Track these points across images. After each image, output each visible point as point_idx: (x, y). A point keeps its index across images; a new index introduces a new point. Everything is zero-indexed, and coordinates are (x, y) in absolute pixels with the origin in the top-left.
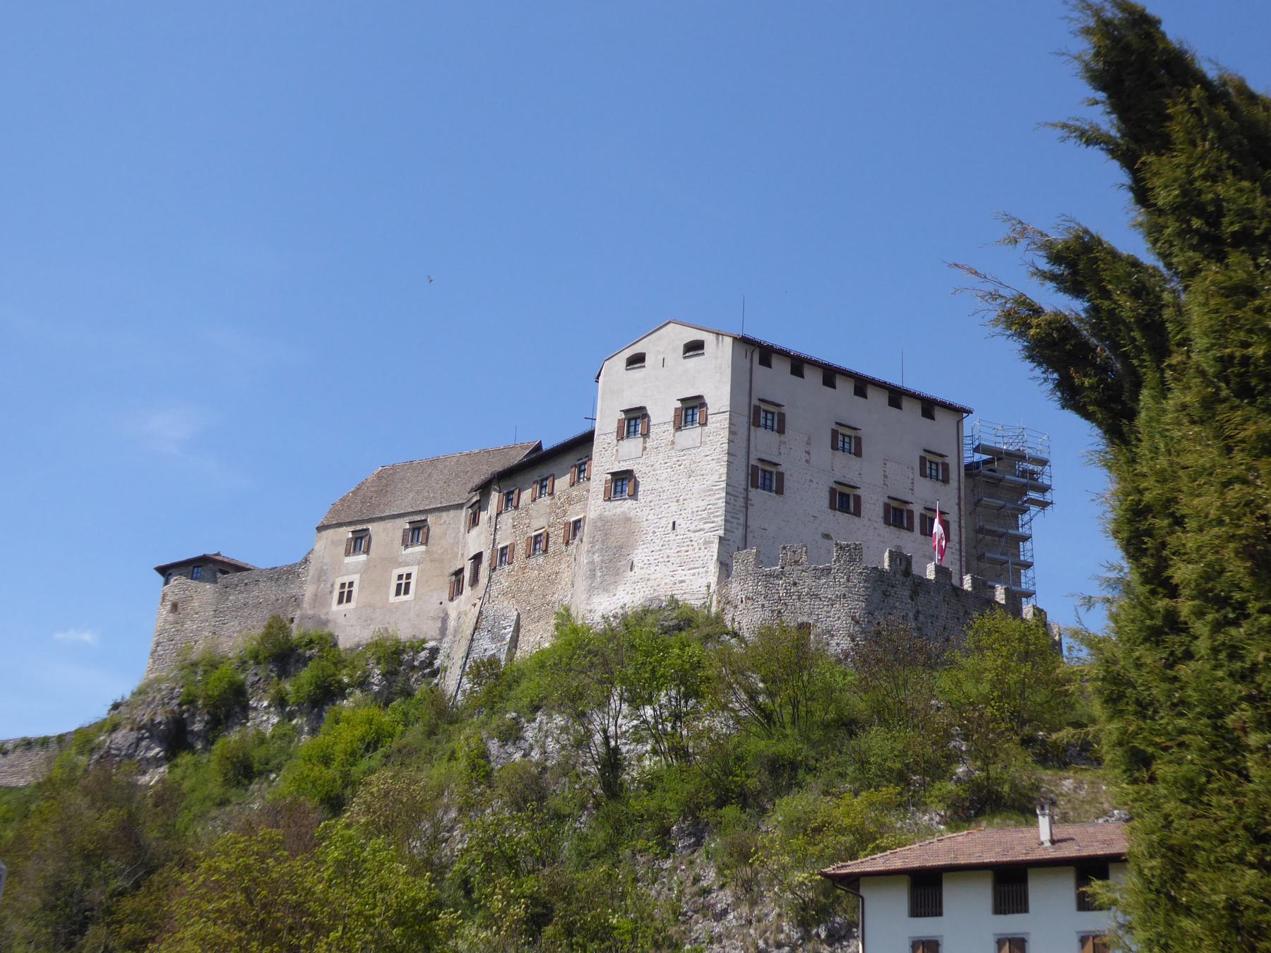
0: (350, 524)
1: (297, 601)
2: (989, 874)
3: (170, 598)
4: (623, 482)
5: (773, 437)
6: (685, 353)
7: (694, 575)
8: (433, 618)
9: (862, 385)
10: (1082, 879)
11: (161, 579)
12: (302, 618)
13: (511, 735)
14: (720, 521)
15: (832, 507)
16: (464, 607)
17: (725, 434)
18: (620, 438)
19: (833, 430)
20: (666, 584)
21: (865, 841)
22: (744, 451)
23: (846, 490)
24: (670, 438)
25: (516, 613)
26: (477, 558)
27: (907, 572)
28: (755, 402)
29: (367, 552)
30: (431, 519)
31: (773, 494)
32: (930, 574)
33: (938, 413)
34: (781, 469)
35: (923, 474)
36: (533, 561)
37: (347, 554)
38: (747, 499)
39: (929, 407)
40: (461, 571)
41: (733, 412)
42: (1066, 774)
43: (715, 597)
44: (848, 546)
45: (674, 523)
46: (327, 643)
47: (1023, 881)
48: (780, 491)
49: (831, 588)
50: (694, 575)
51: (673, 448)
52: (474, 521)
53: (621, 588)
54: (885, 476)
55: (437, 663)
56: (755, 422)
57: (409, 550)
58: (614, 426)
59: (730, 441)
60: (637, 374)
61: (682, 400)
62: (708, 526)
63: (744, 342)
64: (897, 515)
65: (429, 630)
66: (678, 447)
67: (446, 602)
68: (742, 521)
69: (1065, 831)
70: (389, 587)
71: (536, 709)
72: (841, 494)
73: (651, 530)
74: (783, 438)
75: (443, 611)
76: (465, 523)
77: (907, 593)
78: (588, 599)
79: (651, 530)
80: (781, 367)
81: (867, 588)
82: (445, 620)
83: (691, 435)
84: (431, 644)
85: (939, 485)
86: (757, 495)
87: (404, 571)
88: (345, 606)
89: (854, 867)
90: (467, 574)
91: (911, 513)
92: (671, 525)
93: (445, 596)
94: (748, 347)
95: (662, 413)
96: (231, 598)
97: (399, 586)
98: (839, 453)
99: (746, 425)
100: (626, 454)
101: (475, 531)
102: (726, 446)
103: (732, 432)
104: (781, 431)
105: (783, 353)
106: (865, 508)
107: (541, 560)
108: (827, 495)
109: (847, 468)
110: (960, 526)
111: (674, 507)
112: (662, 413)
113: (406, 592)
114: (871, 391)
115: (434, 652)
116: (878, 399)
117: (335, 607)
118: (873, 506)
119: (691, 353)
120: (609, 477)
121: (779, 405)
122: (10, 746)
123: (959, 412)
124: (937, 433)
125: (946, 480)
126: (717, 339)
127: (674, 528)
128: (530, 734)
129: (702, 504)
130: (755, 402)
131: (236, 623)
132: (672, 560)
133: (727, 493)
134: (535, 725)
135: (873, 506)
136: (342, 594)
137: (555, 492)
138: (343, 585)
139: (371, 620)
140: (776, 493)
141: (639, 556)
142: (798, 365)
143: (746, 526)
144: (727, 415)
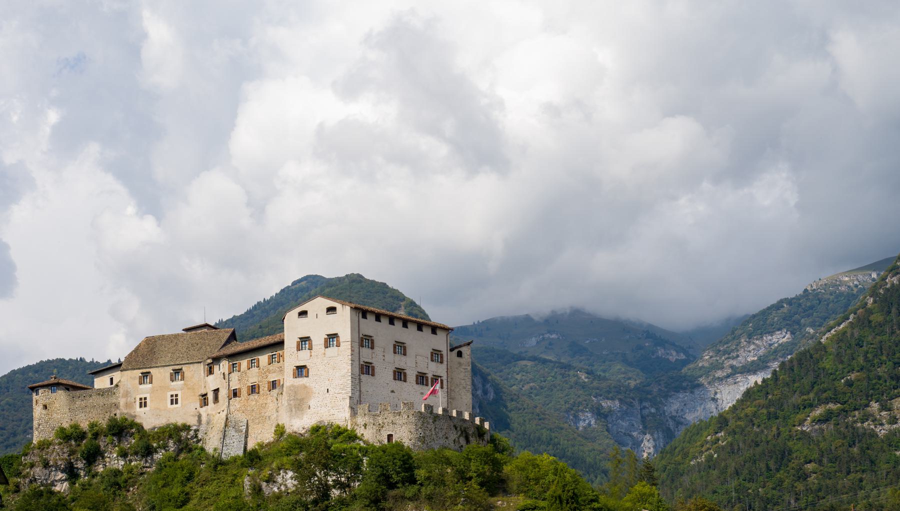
0: (139, 369)
1: (116, 406)
4: (301, 371)
5: (370, 351)
6: (327, 312)
7: (339, 412)
8: (193, 416)
13: (270, 480)
14: (349, 390)
15: (395, 379)
16: (215, 413)
17: (349, 352)
18: (298, 350)
19: (394, 345)
20: (326, 415)
22: (357, 359)
23: (400, 371)
24: (323, 352)
25: (246, 420)
26: (216, 391)
27: (431, 413)
28: (361, 336)
29: (151, 382)
31: (370, 376)
32: (440, 412)
35: (432, 360)
36: (252, 397)
37: (140, 384)
38: (360, 379)
40: (206, 395)
42: (499, 499)
44: (408, 403)
45: (328, 390)
46: (140, 428)
48: (373, 375)
49: (402, 420)
50: (339, 412)
51: (325, 356)
52: (210, 372)
53: (305, 416)
54: (416, 363)
55: (200, 436)
56: (362, 345)
57: (174, 383)
59: (352, 355)
60: (303, 320)
61: (328, 335)
62: (343, 392)
64: (422, 379)
65: (192, 421)
68: (358, 389)
70: (167, 400)
71: (279, 469)
73: (317, 392)
74: (373, 351)
75: (198, 413)
76: (204, 371)
77: (431, 421)
78: (290, 420)
79: (317, 392)
81: (416, 420)
82: (200, 416)
83: (332, 350)
84: (195, 428)
85: (439, 364)
86: (364, 377)
87: (174, 393)
88: (143, 409)
90: (211, 397)
91: (427, 377)
92: (326, 390)
95: (318, 340)
96: (77, 403)
97: (172, 400)
98: (397, 355)
99: (358, 347)
100: (303, 357)
101: (211, 377)
102: (350, 357)
103: (352, 351)
104: (372, 348)
105: (372, 312)
106: (408, 377)
108: (392, 374)
109: (401, 362)
110: (447, 381)
111: (327, 382)
112: (318, 340)
115: (197, 431)
118: (411, 376)
119: (330, 313)
120: (295, 368)
121: (371, 337)
125: (442, 362)
126: (343, 307)
127: (328, 392)
128: (279, 479)
130: (361, 336)
131: (83, 415)
132: (328, 405)
133: (352, 378)
134: (281, 476)
135: (411, 376)
136: (141, 403)
137: (260, 366)
138: (141, 399)
139: (160, 415)
140: (372, 375)
141: (312, 403)
143: (360, 391)
144: (350, 343)
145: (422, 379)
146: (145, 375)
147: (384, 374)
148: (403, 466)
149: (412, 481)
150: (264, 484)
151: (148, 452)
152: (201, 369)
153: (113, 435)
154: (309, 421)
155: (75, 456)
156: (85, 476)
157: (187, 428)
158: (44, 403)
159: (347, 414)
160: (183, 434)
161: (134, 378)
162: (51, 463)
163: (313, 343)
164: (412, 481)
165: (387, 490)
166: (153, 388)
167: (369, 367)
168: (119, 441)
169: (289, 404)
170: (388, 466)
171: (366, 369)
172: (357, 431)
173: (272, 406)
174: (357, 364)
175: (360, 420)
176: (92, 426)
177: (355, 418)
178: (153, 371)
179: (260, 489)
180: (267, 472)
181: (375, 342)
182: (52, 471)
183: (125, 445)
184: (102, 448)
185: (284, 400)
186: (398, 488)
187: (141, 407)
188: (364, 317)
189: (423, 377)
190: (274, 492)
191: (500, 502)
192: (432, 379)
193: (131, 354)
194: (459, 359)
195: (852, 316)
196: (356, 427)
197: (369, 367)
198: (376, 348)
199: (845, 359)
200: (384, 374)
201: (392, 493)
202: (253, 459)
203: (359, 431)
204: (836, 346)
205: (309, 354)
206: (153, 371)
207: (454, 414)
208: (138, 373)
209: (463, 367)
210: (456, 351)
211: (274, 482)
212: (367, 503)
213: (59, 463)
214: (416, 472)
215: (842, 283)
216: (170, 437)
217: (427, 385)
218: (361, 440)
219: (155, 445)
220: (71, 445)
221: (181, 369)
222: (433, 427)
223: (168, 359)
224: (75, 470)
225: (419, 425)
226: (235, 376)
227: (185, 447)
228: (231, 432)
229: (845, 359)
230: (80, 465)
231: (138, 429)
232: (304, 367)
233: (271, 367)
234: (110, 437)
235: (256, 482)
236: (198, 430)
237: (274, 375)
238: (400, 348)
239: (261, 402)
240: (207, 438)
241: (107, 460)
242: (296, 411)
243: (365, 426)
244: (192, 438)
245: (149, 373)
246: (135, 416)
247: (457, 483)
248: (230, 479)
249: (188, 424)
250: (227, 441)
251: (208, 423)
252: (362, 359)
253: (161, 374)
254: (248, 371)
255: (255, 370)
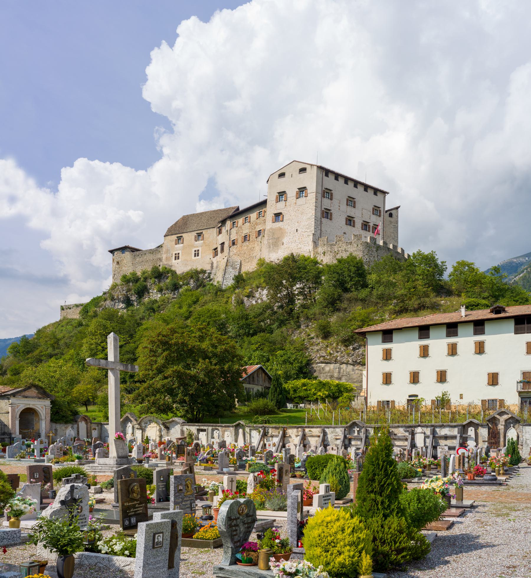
0: (176, 234)
1: (160, 260)
2: (472, 324)
3: (116, 260)
5: (329, 201)
9: (356, 183)
10: (516, 323)
11: (111, 255)
12: (163, 265)
14: (313, 228)
15: (346, 224)
16: (221, 260)
18: (277, 202)
21: (365, 322)
22: (320, 206)
23: (351, 219)
24: (295, 202)
26: (223, 244)
27: (375, 243)
28: (324, 189)
30: (204, 232)
33: (378, 193)
34: (331, 211)
36: (244, 244)
37: (176, 244)
38: (321, 221)
39: (376, 191)
40: (217, 248)
41: (317, 192)
43: (312, 253)
46: (174, 273)
47: (392, 333)
48: (331, 219)
52: (220, 232)
53: (279, 251)
55: (211, 277)
57: (197, 242)
58: (295, 194)
59: (316, 202)
60: (282, 180)
62: (308, 230)
63: (320, 168)
64: (365, 226)
65: (207, 268)
66: (297, 204)
67: (212, 258)
69: (469, 312)
71: (258, 287)
72: (349, 220)
77: (375, 250)
80: (332, 177)
82: (212, 264)
83: (302, 200)
85: (378, 217)
86: (324, 220)
87: (197, 249)
88: (177, 261)
89: (365, 329)
90: (219, 249)
91: (369, 226)
93: (211, 256)
94: (322, 170)
95: (292, 193)
97: (195, 254)
100: (280, 207)
101: (220, 236)
102: (314, 204)
103: (316, 199)
104: (331, 199)
105: (333, 172)
106: (356, 224)
107: (247, 244)
109: (351, 211)
111: (297, 224)
112: (292, 193)
113: (198, 256)
114: (359, 186)
115: (210, 273)
116: (361, 188)
117: (174, 261)
118: (359, 223)
121: (331, 190)
122: (71, 307)
123: (384, 193)
124: (376, 200)
125: (380, 216)
128: (257, 295)
129: (307, 223)
130: (324, 189)
131: (140, 267)
134: (258, 292)
135: (359, 223)
136: (176, 257)
138: (176, 254)
141: (285, 240)
142: (337, 176)
145: (365, 226)
146: (179, 238)
147: (339, 219)
148: (357, 272)
149: (365, 286)
150: (245, 299)
151: (175, 287)
152: (215, 231)
153: (156, 278)
154: (282, 254)
155: (131, 292)
156: (137, 305)
157: (203, 272)
158: (117, 260)
159: (310, 247)
160: (201, 275)
161: (171, 241)
162: (115, 297)
163: (288, 196)
164: (365, 286)
165: (342, 293)
166: (184, 246)
167: (328, 213)
168: (159, 282)
169: (268, 243)
170: (344, 272)
171: (326, 214)
172: (318, 258)
173: (257, 248)
174: (319, 210)
175: (320, 250)
176: (144, 273)
177: (317, 248)
178: (184, 235)
179: (242, 302)
180: (248, 290)
181: (334, 195)
182: (116, 302)
183: (162, 284)
184: (149, 287)
185: (265, 241)
186: (352, 292)
187: (175, 259)
188: (327, 175)
189: (366, 225)
190: (252, 305)
191: (443, 302)
192: (373, 227)
193: (172, 226)
194: (390, 219)
195: (525, 271)
196: (317, 255)
197: (328, 213)
198: (334, 200)
199: (527, 287)
200: (339, 219)
201: (348, 295)
202: (239, 281)
203: (319, 259)
204: (522, 282)
205: (284, 205)
206: (184, 235)
207: (391, 247)
208: (174, 237)
209: (393, 224)
210: (388, 213)
211: (253, 297)
212: (325, 304)
213: (120, 297)
214: (368, 277)
215: (513, 262)
216: (192, 277)
217: (369, 231)
218: (321, 264)
219: (181, 283)
220: (129, 286)
221: (202, 233)
222: (376, 255)
223: (194, 227)
224: (131, 302)
225: (366, 252)
226: (234, 231)
227: (200, 284)
228: (230, 269)
229: (527, 287)
230: (134, 298)
231: (172, 274)
232: (281, 213)
233: (258, 221)
234: (153, 279)
235: (240, 298)
236: (211, 273)
237: (260, 226)
238: (351, 201)
239: (250, 246)
240: (216, 277)
241: (151, 294)
242: (273, 248)
243: (324, 253)
244: (206, 278)
245: (182, 236)
246: (171, 266)
247: (408, 282)
248: (225, 300)
249: (205, 269)
250: (227, 276)
251: (217, 267)
252: (323, 207)
253: (189, 237)
254: (243, 226)
255: (247, 224)
